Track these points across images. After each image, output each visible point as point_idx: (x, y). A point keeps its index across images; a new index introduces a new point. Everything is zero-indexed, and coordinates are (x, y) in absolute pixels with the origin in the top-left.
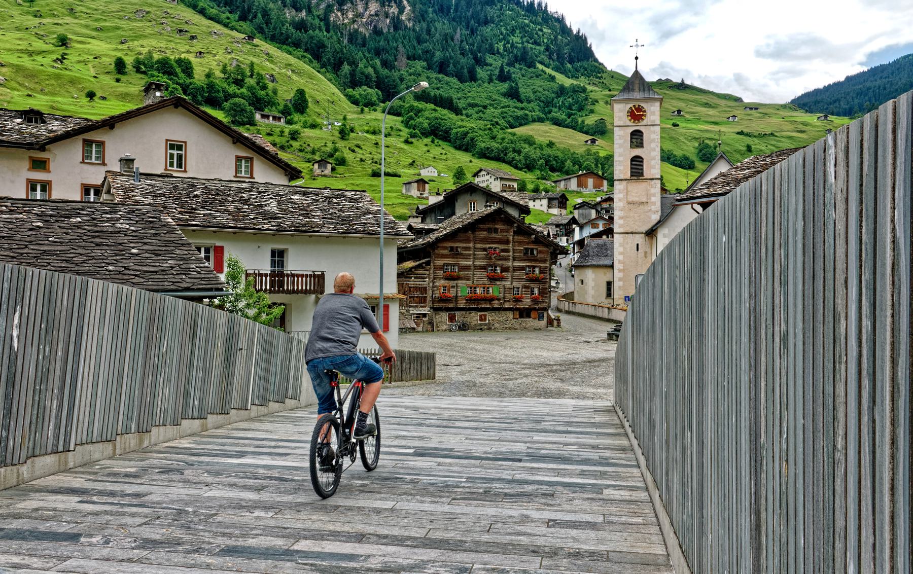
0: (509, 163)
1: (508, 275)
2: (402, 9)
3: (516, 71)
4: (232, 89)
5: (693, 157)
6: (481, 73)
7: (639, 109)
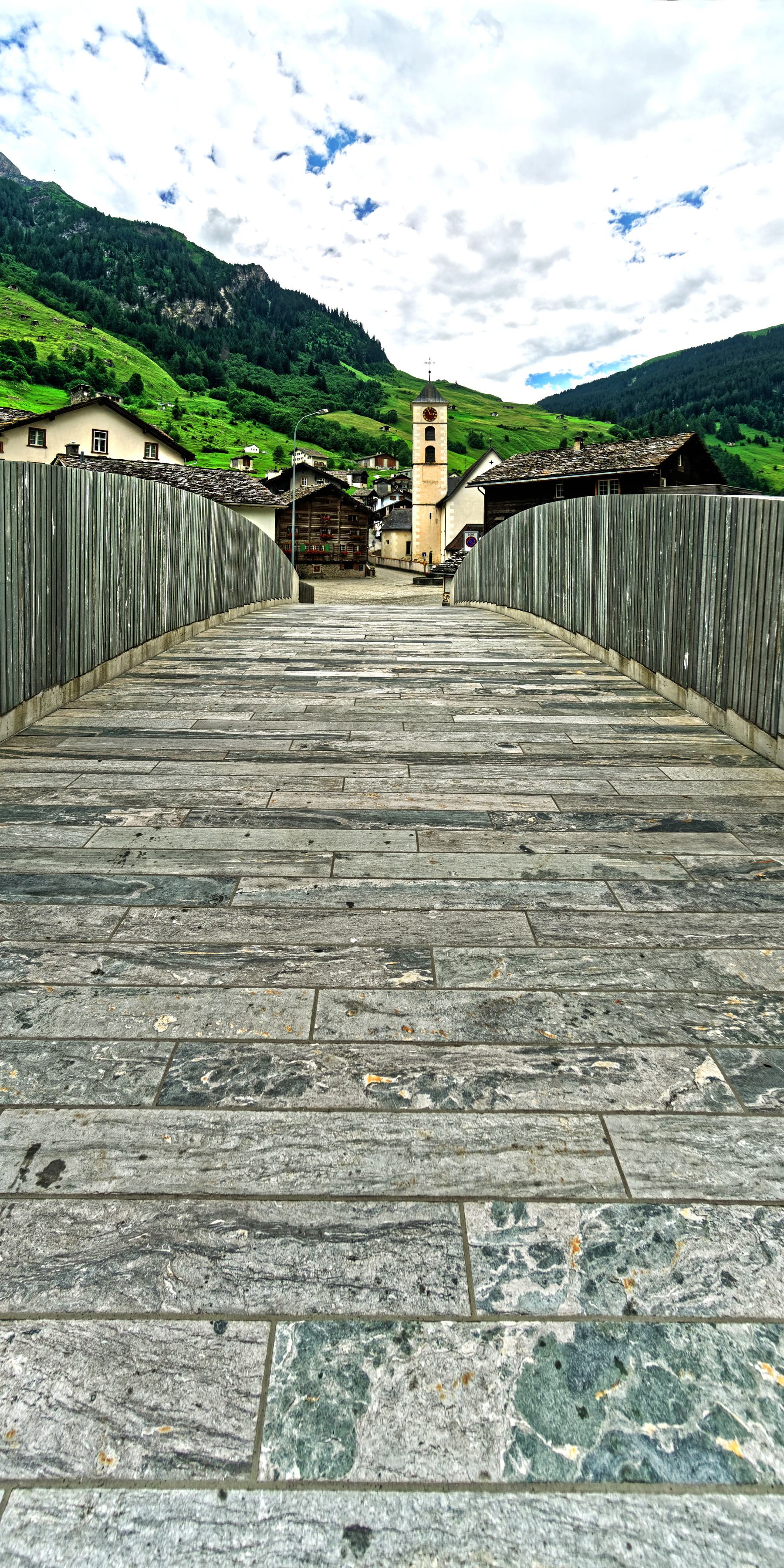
0: (320, 444)
1: (337, 536)
2: (225, 309)
3: (323, 367)
4: (73, 371)
5: (465, 444)
6: (294, 367)
7: (433, 411)
